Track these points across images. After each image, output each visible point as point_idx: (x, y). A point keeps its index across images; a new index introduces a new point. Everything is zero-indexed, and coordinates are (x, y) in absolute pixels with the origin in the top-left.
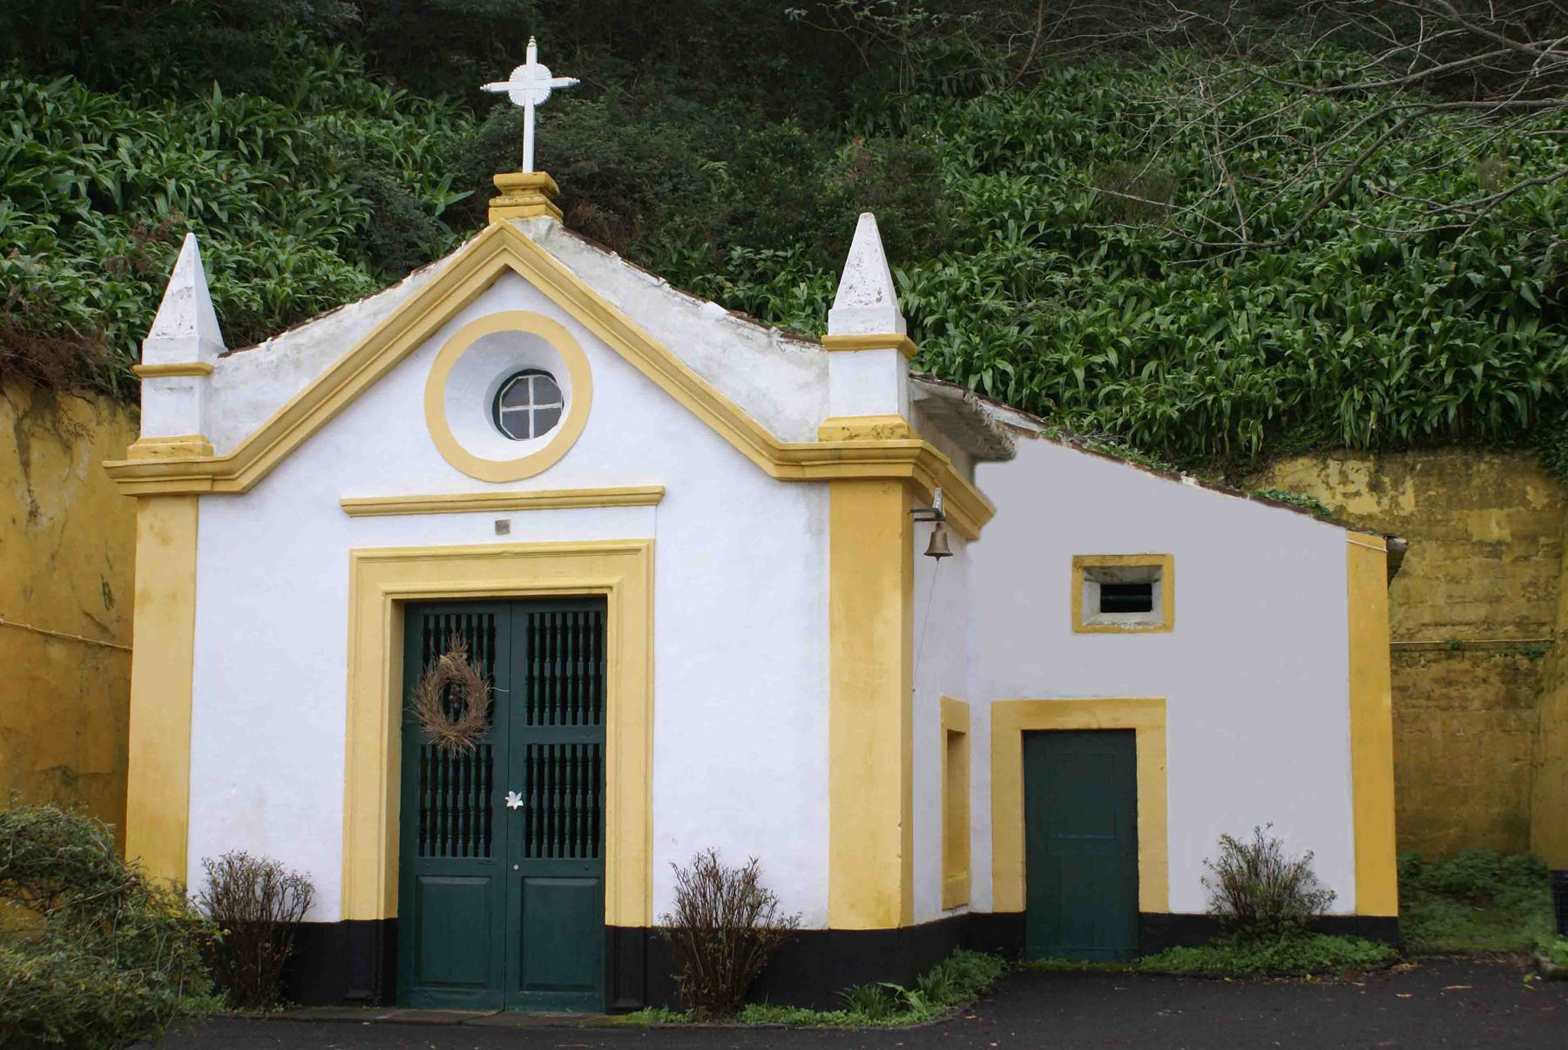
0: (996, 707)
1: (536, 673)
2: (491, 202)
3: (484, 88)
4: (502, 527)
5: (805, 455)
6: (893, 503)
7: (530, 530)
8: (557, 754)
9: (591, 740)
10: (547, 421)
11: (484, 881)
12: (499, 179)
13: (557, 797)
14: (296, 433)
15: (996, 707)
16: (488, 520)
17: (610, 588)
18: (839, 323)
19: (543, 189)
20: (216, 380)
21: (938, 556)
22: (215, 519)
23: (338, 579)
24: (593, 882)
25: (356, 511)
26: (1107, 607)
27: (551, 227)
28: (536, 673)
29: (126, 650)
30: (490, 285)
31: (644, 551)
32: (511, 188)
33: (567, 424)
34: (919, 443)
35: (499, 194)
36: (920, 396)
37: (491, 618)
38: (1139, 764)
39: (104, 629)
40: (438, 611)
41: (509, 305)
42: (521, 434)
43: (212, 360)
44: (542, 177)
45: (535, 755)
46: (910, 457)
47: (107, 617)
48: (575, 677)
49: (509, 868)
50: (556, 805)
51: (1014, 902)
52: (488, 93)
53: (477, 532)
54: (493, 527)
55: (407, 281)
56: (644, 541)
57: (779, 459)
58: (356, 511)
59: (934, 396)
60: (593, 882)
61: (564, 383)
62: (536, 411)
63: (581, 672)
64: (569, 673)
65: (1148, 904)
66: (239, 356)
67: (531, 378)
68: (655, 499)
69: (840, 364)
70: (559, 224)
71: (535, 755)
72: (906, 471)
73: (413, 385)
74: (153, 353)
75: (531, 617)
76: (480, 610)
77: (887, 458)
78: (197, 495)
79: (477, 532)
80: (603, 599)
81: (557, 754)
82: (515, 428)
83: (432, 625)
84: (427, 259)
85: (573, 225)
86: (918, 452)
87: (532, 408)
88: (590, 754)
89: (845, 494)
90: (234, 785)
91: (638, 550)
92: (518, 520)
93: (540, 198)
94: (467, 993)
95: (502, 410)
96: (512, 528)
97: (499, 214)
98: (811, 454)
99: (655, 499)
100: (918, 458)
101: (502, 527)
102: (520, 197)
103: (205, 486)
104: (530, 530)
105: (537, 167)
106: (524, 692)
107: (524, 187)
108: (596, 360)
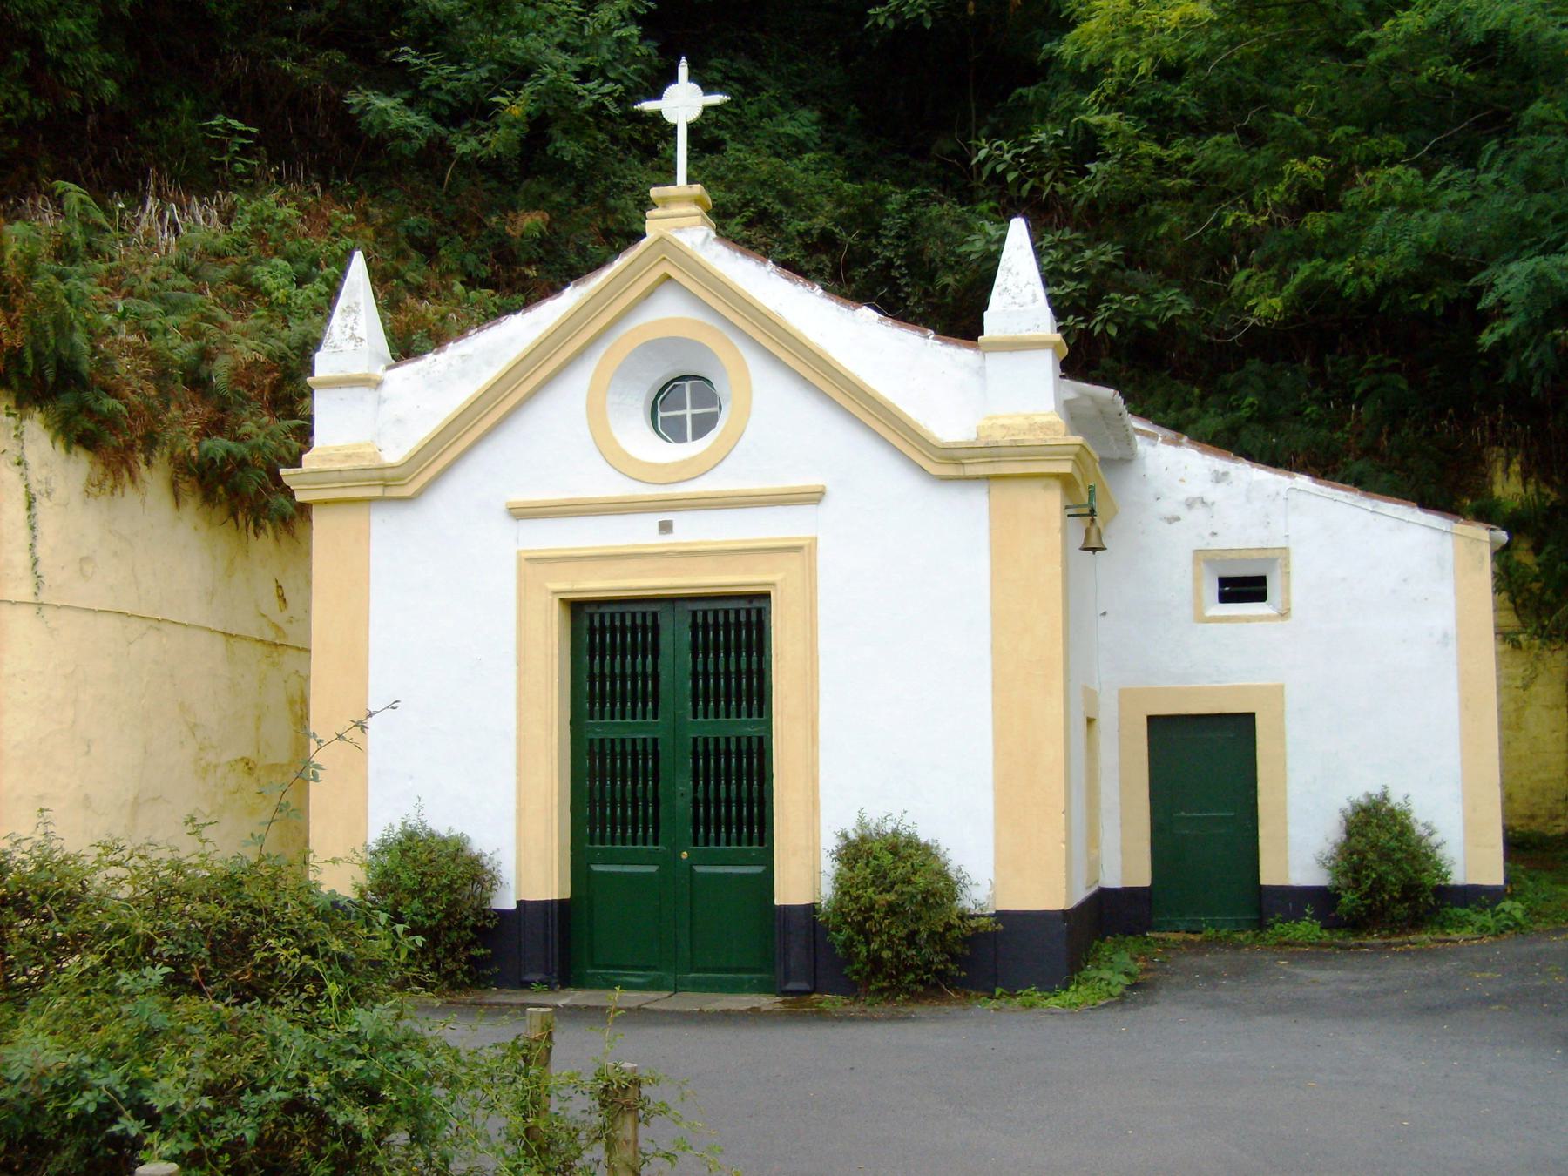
0: (1123, 693)
1: (700, 668)
2: (648, 213)
3: (638, 107)
4: (666, 527)
5: (964, 453)
6: (1051, 502)
7: (692, 530)
8: (722, 746)
9: (753, 731)
10: (704, 425)
11: (653, 869)
12: (654, 192)
13: (723, 786)
14: (468, 435)
15: (1123, 693)
16: (655, 519)
17: (773, 584)
18: (998, 318)
19: (698, 201)
20: (386, 390)
21: (1094, 550)
22: (384, 527)
23: (506, 581)
24: (758, 869)
25: (520, 513)
26: (1224, 598)
27: (708, 236)
28: (700, 668)
29: (303, 649)
30: (649, 294)
31: (806, 549)
32: (666, 201)
33: (725, 430)
34: (1078, 440)
35: (655, 206)
36: (1071, 395)
37: (655, 615)
38: (1260, 745)
39: (278, 628)
40: (607, 610)
41: (668, 312)
42: (679, 437)
43: (379, 371)
44: (697, 189)
45: (701, 749)
46: (1068, 454)
47: (280, 618)
48: (602, 675)
49: (677, 857)
50: (723, 795)
51: (1140, 875)
52: (642, 112)
53: (640, 532)
54: (657, 527)
55: (568, 291)
56: (805, 539)
57: (940, 458)
58: (520, 513)
59: (1084, 395)
60: (758, 869)
61: (721, 388)
62: (693, 416)
63: (744, 666)
64: (618, 670)
65: (1268, 877)
66: (410, 369)
67: (688, 384)
68: (814, 497)
69: (998, 363)
70: (713, 234)
71: (701, 749)
72: (1066, 468)
73: (576, 388)
74: (325, 364)
75: (694, 614)
76: (638, 608)
77: (1052, 455)
78: (369, 500)
79: (640, 532)
80: (766, 596)
81: (722, 746)
82: (673, 431)
83: (597, 623)
84: (574, 274)
85: (724, 235)
86: (1078, 448)
87: (688, 412)
88: (755, 746)
89: (998, 489)
90: (411, 777)
91: (798, 549)
92: (679, 520)
93: (696, 209)
94: (639, 976)
95: (660, 414)
96: (675, 527)
97: (655, 225)
98: (970, 452)
99: (814, 497)
100: (1077, 455)
101: (666, 527)
102: (675, 210)
103: (377, 492)
104: (692, 530)
105: (691, 180)
106: (662, 688)
107: (679, 200)
108: (755, 365)
